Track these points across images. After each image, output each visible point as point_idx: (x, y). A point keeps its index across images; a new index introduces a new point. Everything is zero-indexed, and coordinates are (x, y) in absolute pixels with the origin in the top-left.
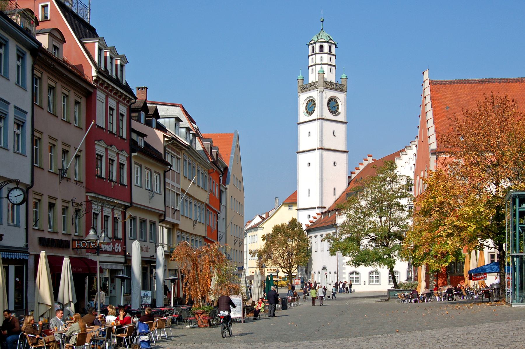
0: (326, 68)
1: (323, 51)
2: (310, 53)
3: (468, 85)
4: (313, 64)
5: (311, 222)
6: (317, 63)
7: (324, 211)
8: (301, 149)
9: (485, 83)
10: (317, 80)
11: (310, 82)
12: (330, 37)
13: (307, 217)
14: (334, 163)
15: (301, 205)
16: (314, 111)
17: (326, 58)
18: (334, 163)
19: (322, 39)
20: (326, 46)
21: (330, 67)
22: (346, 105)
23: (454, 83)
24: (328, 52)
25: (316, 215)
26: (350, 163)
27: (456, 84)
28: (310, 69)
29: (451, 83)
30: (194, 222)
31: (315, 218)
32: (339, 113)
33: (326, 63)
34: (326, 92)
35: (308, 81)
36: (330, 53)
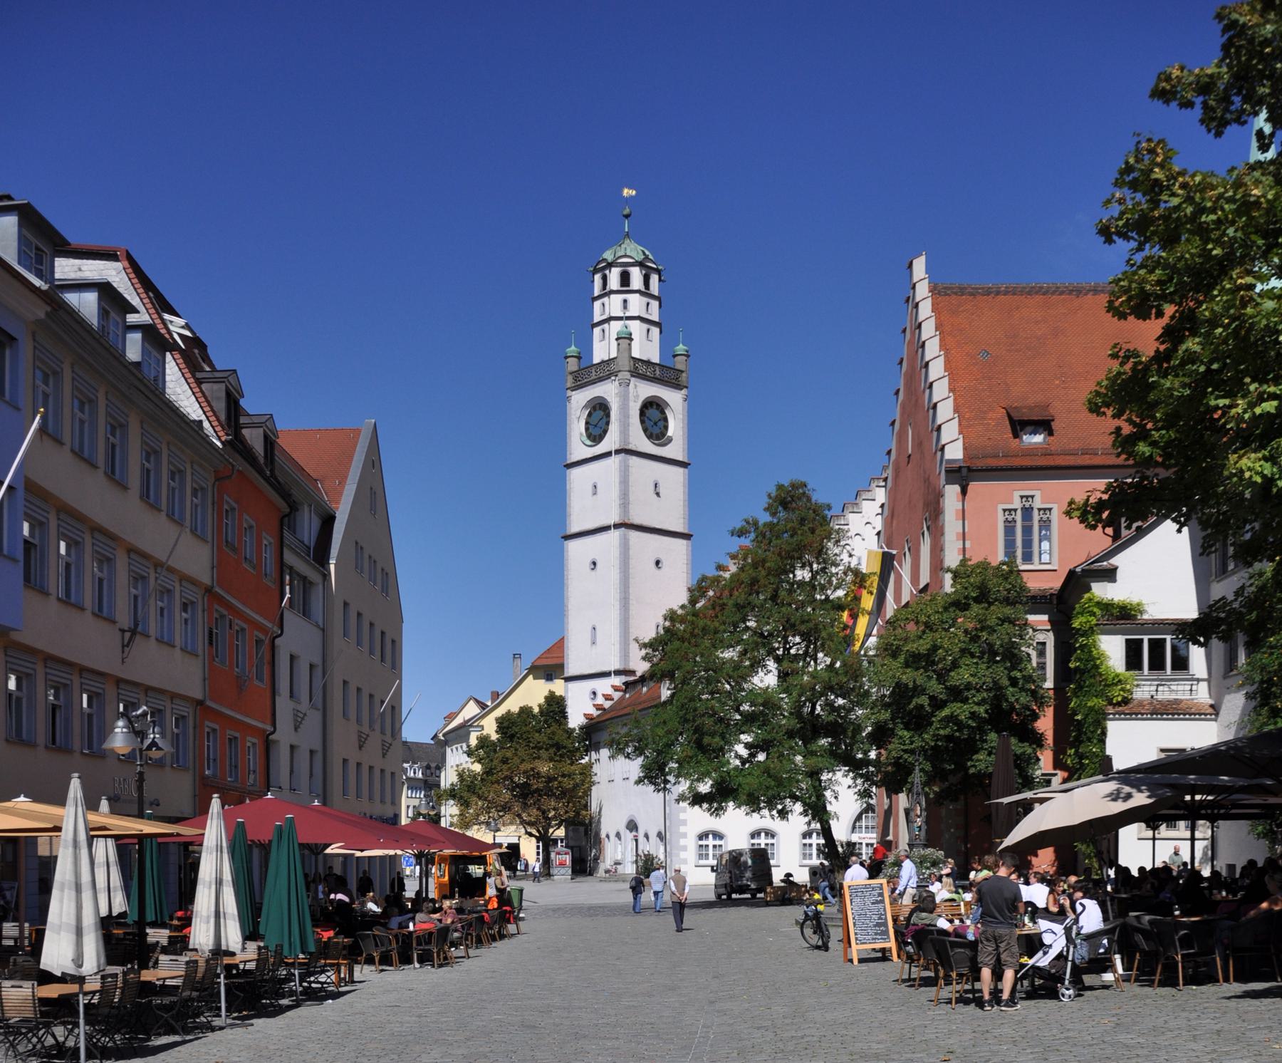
0: (636, 328)
1: (628, 286)
2: (596, 293)
3: (1039, 298)
4: (604, 317)
5: (598, 707)
6: (613, 315)
7: (632, 678)
8: (574, 529)
9: (1086, 294)
10: (613, 355)
11: (596, 360)
12: (647, 253)
13: (588, 695)
14: (658, 563)
15: (571, 670)
16: (605, 432)
17: (637, 304)
18: (658, 563)
19: (625, 256)
20: (636, 276)
21: (645, 326)
22: (686, 422)
23: (998, 293)
24: (643, 289)
25: (610, 691)
26: (695, 559)
27: (1005, 295)
28: (597, 331)
29: (990, 293)
30: (127, 635)
31: (607, 697)
32: (670, 440)
33: (636, 315)
34: (636, 386)
35: (592, 358)
36: (645, 293)
